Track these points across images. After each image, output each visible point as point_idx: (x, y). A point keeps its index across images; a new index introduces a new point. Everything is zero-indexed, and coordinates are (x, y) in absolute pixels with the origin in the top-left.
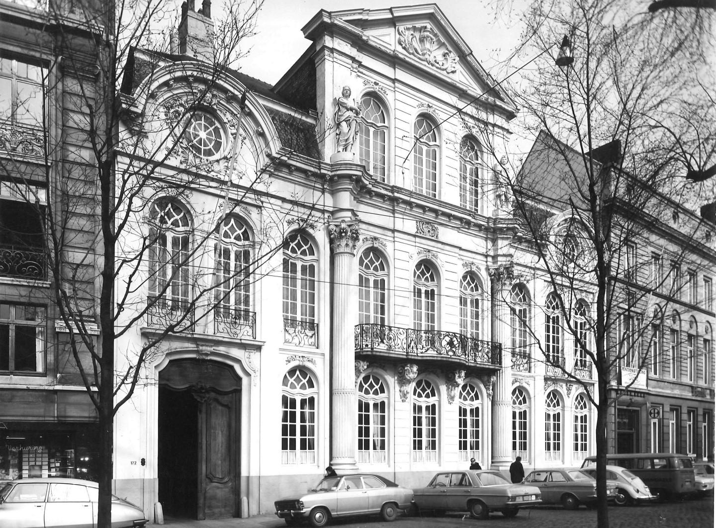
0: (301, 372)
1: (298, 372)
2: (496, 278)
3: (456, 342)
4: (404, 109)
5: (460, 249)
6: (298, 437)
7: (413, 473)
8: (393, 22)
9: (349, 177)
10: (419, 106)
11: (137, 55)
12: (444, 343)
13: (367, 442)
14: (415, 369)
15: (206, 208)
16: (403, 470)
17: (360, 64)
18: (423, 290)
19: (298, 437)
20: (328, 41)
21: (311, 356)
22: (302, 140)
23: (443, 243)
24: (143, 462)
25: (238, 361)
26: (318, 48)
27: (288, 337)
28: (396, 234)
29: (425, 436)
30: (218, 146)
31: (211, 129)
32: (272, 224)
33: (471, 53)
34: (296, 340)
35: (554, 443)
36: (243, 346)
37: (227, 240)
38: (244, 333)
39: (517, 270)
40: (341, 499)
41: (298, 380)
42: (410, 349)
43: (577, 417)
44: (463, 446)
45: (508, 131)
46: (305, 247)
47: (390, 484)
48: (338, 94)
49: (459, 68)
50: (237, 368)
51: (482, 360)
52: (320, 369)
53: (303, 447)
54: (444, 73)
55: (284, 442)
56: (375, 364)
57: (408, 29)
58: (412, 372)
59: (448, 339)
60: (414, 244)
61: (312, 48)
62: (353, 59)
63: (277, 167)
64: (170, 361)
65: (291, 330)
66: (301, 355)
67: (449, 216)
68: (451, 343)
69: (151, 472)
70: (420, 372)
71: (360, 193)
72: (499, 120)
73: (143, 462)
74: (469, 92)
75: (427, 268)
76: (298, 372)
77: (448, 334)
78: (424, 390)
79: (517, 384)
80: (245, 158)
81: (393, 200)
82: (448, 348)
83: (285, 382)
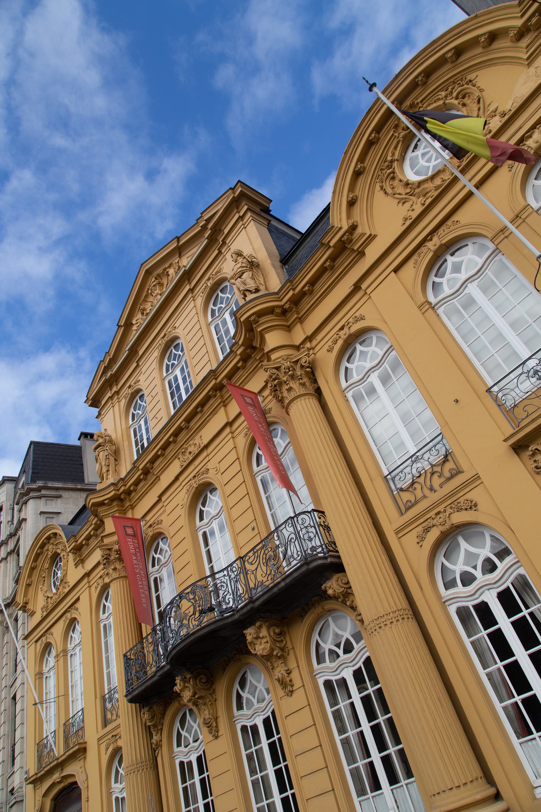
60: (366, 298)
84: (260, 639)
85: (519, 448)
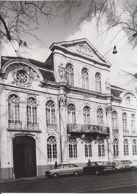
0: (51, 138)
1: (51, 138)
2: (107, 110)
3: (95, 128)
4: (78, 66)
5: (97, 103)
6: (52, 155)
7: (49, 165)
8: (74, 45)
9: (63, 86)
10: (82, 66)
11: (3, 58)
12: (92, 128)
13: (101, 154)
14: (84, 135)
15: (23, 97)
16: (42, 164)
17: (66, 57)
18: (86, 114)
19: (52, 155)
20: (56, 51)
21: (55, 133)
22: (49, 77)
23: (91, 102)
24: (9, 163)
25: (34, 136)
26: (54, 52)
27: (48, 128)
28: (108, 104)
29: (88, 152)
30: (26, 81)
31: (24, 76)
32: (42, 100)
33: (97, 51)
34: (51, 129)
35: (126, 153)
36: (36, 132)
37: (49, 107)
38: (36, 129)
39: (113, 108)
40: (62, 171)
41: (52, 140)
42: (82, 130)
43: (133, 146)
44: (86, 156)
45: (109, 71)
46: (73, 108)
47: (76, 166)
48: (59, 65)
49: (94, 55)
50: (34, 137)
51: (104, 132)
52: (57, 137)
53: (54, 157)
54: (90, 57)
55: (70, 155)
56: (74, 135)
57: (79, 46)
58: (83, 136)
59: (93, 127)
61: (52, 52)
62: (64, 55)
63: (44, 85)
64: (16, 137)
65: (49, 127)
66: (52, 133)
67: (92, 94)
68: (94, 128)
69: (11, 166)
70: (86, 136)
71: (67, 89)
72: (106, 68)
73: (9, 163)
74: (68, 50)
75: (87, 108)
76: (51, 138)
77: (93, 126)
78: (88, 141)
79: (115, 138)
80: (36, 83)
81: (76, 91)
82: (93, 129)
83: (48, 140)
84: (83, 136)
85: (123, 136)
